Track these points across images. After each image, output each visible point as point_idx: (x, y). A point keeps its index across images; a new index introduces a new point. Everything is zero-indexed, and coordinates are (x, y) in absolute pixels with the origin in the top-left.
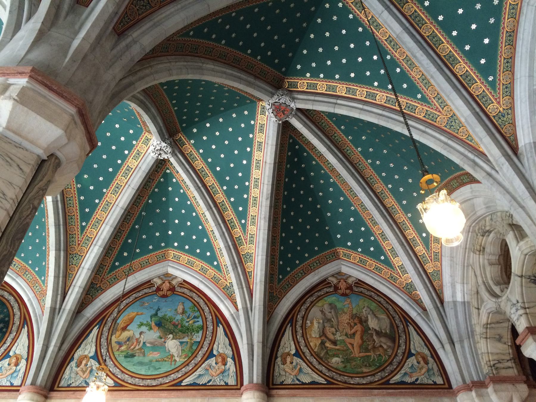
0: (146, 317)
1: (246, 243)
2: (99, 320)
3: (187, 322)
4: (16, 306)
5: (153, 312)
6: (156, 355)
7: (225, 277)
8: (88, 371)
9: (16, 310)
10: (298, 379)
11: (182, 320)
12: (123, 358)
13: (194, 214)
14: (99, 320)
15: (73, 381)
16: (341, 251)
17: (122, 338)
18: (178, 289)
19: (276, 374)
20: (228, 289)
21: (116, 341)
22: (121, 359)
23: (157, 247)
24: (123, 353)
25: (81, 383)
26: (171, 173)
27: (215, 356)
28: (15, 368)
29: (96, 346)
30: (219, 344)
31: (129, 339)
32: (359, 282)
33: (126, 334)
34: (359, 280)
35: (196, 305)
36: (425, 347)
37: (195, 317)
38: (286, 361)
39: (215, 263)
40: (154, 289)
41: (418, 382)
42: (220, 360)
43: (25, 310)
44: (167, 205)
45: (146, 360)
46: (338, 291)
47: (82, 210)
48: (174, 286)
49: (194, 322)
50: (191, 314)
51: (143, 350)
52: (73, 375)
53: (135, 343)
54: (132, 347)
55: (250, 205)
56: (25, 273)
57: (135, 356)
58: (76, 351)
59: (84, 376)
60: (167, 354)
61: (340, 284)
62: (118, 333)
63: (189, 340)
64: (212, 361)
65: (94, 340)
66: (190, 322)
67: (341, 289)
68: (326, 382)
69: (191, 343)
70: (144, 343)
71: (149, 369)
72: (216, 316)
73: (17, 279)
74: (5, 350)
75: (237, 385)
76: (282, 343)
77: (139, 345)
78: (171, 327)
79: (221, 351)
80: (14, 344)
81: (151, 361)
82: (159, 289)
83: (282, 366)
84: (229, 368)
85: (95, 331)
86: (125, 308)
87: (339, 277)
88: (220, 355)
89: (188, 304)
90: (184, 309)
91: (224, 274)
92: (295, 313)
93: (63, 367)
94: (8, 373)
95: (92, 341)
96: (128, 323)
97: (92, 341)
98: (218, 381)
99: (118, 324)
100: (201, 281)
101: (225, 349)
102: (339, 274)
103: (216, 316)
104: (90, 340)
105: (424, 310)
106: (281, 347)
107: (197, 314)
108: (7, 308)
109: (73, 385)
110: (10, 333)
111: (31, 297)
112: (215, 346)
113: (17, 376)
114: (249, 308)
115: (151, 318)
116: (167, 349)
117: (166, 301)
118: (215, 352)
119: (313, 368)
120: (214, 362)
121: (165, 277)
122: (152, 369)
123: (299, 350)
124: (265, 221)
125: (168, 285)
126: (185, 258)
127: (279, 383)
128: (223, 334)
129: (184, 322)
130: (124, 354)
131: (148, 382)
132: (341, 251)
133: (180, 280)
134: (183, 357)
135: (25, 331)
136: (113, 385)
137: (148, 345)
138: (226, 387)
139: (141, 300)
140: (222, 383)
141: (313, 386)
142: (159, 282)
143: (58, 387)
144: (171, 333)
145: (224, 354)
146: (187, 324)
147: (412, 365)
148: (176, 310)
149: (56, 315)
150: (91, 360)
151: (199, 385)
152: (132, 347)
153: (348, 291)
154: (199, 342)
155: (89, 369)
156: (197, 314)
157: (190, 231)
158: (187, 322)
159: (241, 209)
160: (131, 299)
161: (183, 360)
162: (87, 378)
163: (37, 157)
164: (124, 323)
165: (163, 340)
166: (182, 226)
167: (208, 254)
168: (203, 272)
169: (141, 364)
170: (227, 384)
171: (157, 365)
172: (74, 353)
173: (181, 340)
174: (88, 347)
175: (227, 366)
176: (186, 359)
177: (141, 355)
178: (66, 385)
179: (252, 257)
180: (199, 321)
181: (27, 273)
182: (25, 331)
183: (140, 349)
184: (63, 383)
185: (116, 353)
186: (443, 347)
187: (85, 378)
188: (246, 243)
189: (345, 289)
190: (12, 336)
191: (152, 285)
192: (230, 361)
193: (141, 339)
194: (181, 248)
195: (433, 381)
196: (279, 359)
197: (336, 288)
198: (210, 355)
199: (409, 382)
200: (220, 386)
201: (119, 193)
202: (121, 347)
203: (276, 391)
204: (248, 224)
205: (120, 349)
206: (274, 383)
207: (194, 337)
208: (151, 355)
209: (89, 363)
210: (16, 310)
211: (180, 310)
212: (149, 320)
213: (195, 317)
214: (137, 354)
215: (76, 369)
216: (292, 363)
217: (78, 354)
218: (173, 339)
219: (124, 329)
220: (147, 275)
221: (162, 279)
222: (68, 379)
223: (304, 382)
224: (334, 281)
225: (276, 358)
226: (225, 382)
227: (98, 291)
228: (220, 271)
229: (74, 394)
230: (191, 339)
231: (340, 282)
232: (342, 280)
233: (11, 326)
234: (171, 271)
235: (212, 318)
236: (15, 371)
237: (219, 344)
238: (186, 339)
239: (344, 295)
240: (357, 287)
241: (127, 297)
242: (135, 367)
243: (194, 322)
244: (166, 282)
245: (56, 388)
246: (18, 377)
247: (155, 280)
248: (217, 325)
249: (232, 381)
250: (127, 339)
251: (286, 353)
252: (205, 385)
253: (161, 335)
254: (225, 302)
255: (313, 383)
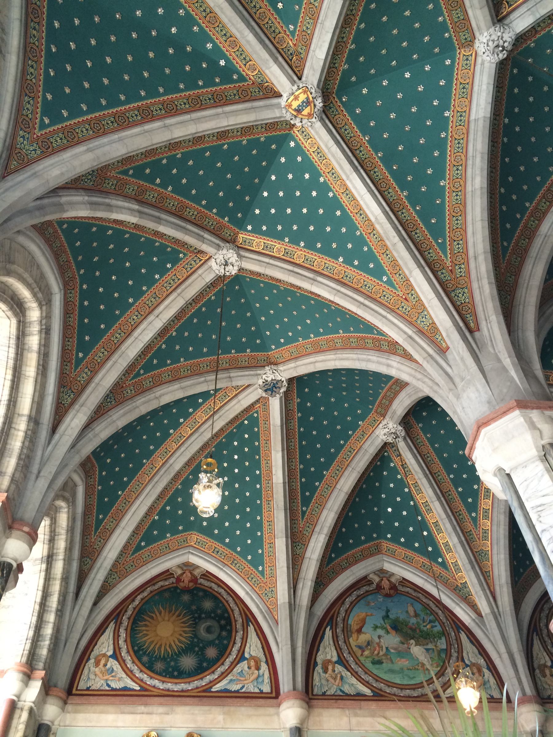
0: (376, 618)
1: (479, 539)
2: (327, 621)
3: (424, 626)
4: (230, 600)
5: (384, 613)
6: (404, 663)
7: (454, 576)
8: (339, 678)
9: (232, 605)
10: (341, 690)
11: (418, 623)
12: (371, 664)
13: (412, 503)
14: (327, 621)
15: (327, 689)
16: (385, 545)
17: (361, 642)
18: (400, 588)
19: (540, 688)
20: (460, 591)
21: (356, 644)
22: (369, 665)
23: (370, 539)
24: (369, 659)
25: (336, 691)
26: (389, 456)
27: (246, 659)
28: (256, 672)
29: (336, 649)
30: (250, 646)
31: (368, 643)
32: (207, 574)
33: (363, 638)
34: (403, 579)
35: (426, 607)
36: (480, 656)
37: (431, 622)
38: (545, 673)
39: (440, 560)
40: (374, 586)
41: (243, 690)
42: (252, 663)
43: (242, 606)
44: (379, 491)
45: (396, 667)
46: (382, 590)
47: (303, 494)
48: (395, 585)
49: (432, 627)
50: (426, 618)
51: (389, 657)
52: (324, 682)
53: (377, 648)
54: (376, 652)
55: (481, 497)
56: (233, 562)
57: (383, 663)
58: (316, 654)
59: (337, 683)
60: (416, 662)
61: (184, 575)
62: (355, 636)
63: (434, 647)
64: (244, 665)
65: (331, 642)
66: (428, 627)
67: (384, 588)
68: (138, 688)
69: (437, 650)
70: (387, 648)
71: (404, 678)
72: (453, 620)
73: (224, 569)
74: (239, 651)
75: (271, 693)
76: (99, 643)
77: (382, 650)
78: (409, 632)
79: (253, 654)
80: (245, 645)
81: (402, 669)
82: (379, 587)
83: (93, 669)
84: (263, 674)
85: (328, 633)
86: (351, 607)
87: (185, 568)
88: (252, 657)
89: (418, 607)
90: (415, 611)
91: (453, 573)
92: (536, 620)
93: (80, 665)
94: (252, 678)
95: (329, 644)
96: (361, 625)
97: (329, 644)
98: (252, 688)
99: (351, 626)
100: (426, 580)
101: (476, 659)
102: (382, 572)
103: (453, 620)
104: (328, 643)
105: (479, 614)
106: (534, 658)
107: (432, 617)
108: (221, 602)
109: (328, 693)
110: (236, 632)
111: (248, 591)
112: (247, 649)
113: (263, 681)
114: (497, 613)
115: (384, 621)
116: (414, 656)
117: (392, 601)
118: (247, 655)
119: (358, 678)
120: (246, 666)
121: (381, 573)
122: (406, 678)
123: (342, 657)
124: (505, 516)
125: (189, 575)
126: (401, 551)
127: (546, 697)
128: (469, 641)
129: (422, 627)
130: (370, 659)
131: (408, 692)
132: (385, 545)
133: (398, 577)
134: (435, 665)
135: (251, 629)
136: (372, 694)
137: (392, 651)
138: (260, 696)
139: (365, 599)
140: (257, 690)
141: (359, 697)
142: (179, 572)
143: (77, 690)
144: (412, 638)
145: (256, 657)
146: (425, 629)
147: (242, 671)
148: (407, 612)
149: (293, 612)
150: (110, 659)
151: (230, 692)
152: (376, 652)
153: (392, 592)
154: (446, 650)
155: (339, 676)
156: (432, 617)
157: (404, 521)
158: (424, 626)
159: (307, 494)
160: (353, 597)
161: (436, 669)
162: (340, 685)
163: (20, 413)
164: (357, 624)
165: (406, 645)
166: (397, 514)
167: (430, 549)
168: (423, 569)
169: (392, 671)
170: (262, 692)
171: (411, 673)
172: (316, 657)
173: (425, 647)
174: (328, 650)
175: (261, 672)
176: (439, 669)
177: (389, 662)
178: (85, 688)
179: (488, 555)
180: (436, 626)
181: (236, 562)
182: (251, 629)
183: (385, 655)
184: (82, 685)
185: (361, 658)
186: (500, 657)
187: (338, 685)
188: (479, 539)
189: (389, 589)
190: (240, 634)
191: (370, 583)
192: (264, 667)
193: (382, 644)
194: (396, 540)
195: (490, 695)
196: (92, 661)
197: (379, 587)
198: (241, 658)
199: (233, 690)
200: (254, 693)
201: (339, 476)
202: (363, 651)
203: (316, 701)
204: (480, 517)
205: (364, 654)
206: (314, 693)
207: (438, 643)
208: (400, 663)
209: (336, 669)
210: (232, 605)
211: (412, 613)
212: (382, 622)
213: (431, 622)
214: (384, 661)
215: (324, 675)
216: (105, 665)
217: (96, 652)
218: (416, 645)
219: (359, 631)
220: (364, 570)
221: (379, 576)
222: (321, 687)
223: (114, 687)
224: (376, 579)
225: (89, 659)
226: (260, 689)
227: (320, 586)
228: (447, 569)
229: (336, 702)
230: (436, 646)
231: (184, 573)
232: (384, 579)
233: (234, 624)
234: (388, 567)
235: (337, 617)
236: (259, 676)
237: (250, 646)
238: (430, 646)
239: (387, 596)
240: (403, 586)
241: (348, 594)
242: (387, 675)
243: (432, 627)
244: (187, 572)
245: (74, 691)
246: (265, 683)
247: (371, 576)
248: (459, 632)
249: (266, 688)
250: (366, 643)
251: (542, 665)
252: (237, 692)
253: (403, 641)
254: (461, 605)
255: (125, 689)
